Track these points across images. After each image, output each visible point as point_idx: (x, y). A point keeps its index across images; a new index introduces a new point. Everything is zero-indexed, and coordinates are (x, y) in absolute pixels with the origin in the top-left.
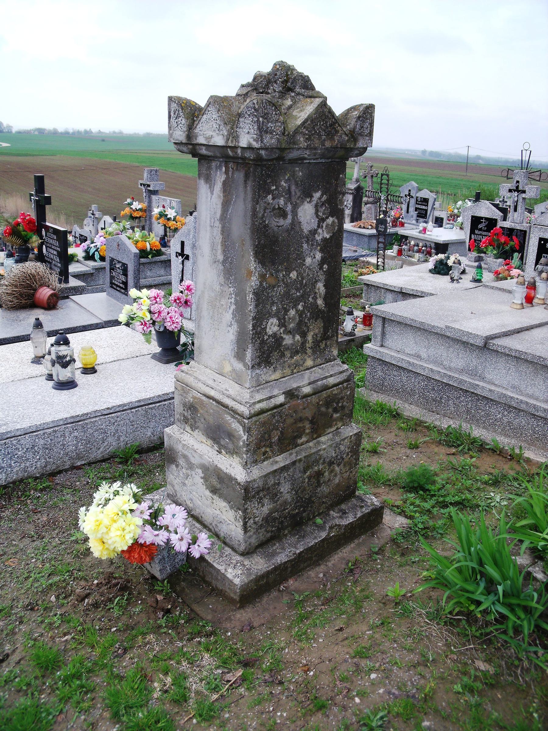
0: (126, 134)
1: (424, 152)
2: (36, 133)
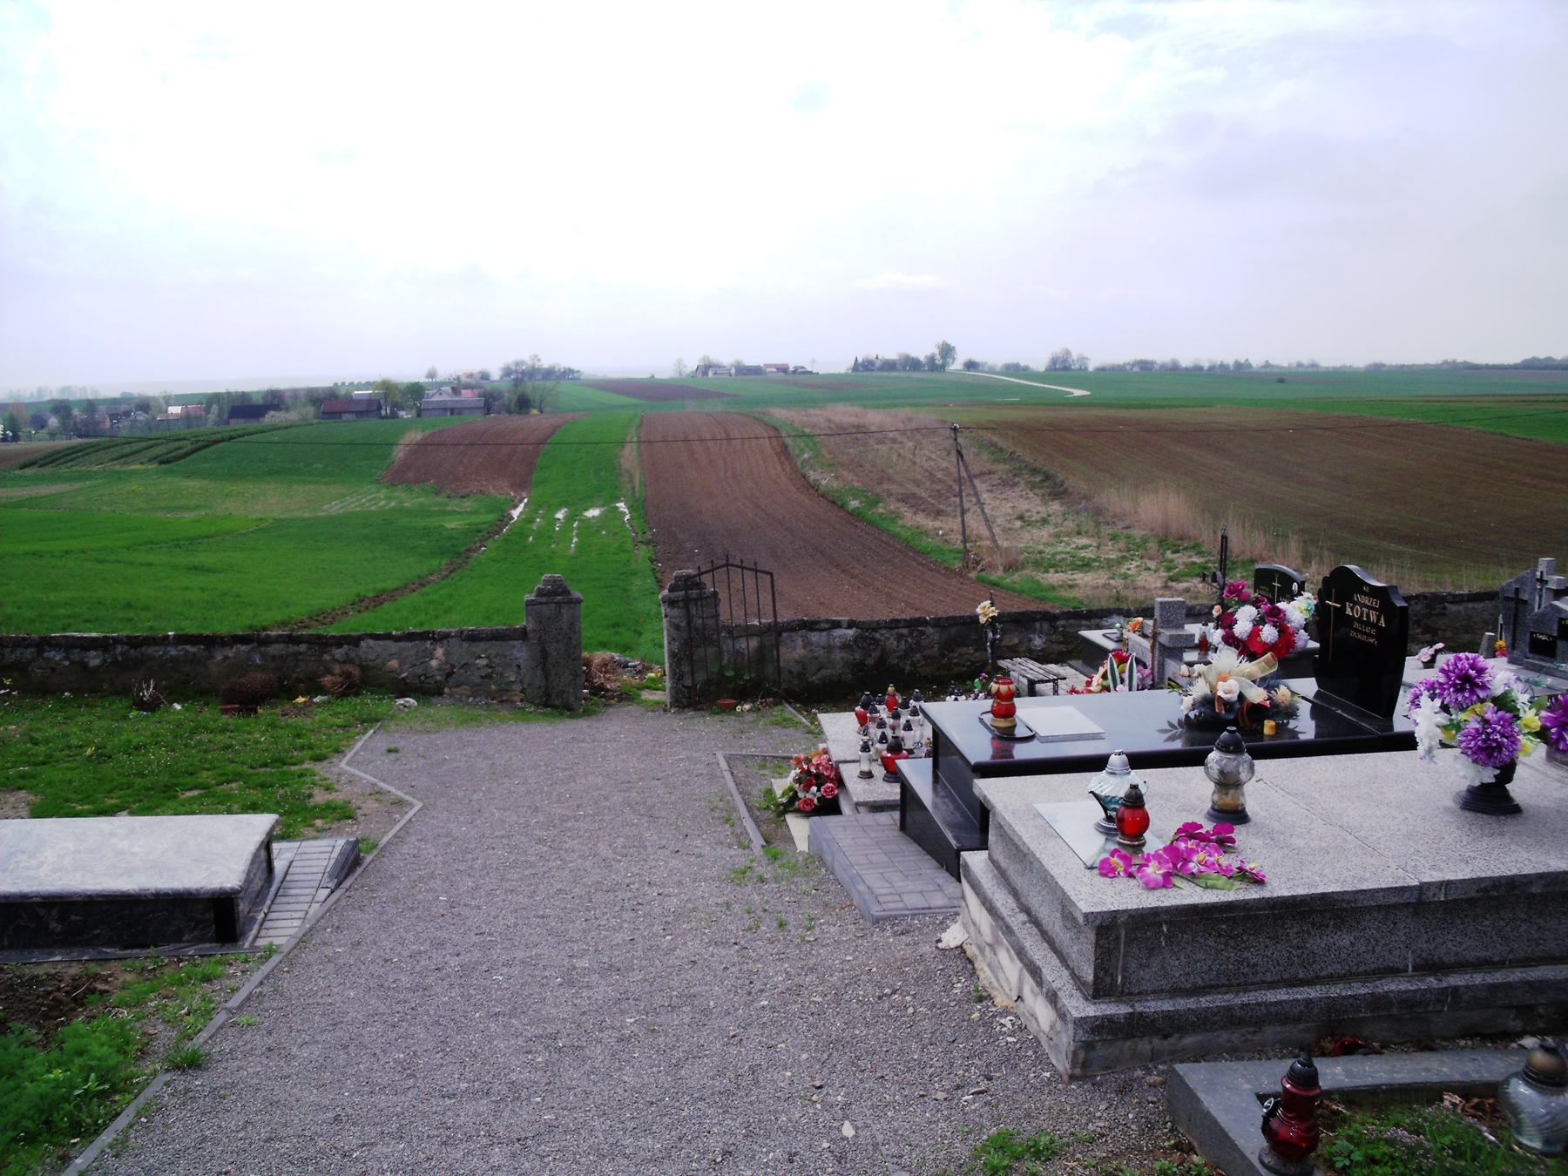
1: (1061, 368)
2: (1137, 369)
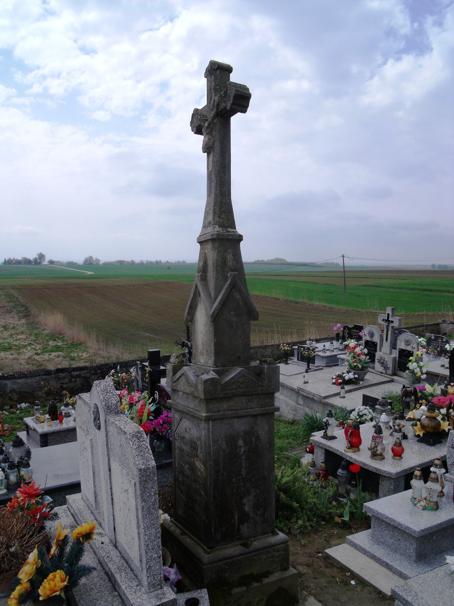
0: (188, 263)
1: (433, 266)
2: (118, 264)
